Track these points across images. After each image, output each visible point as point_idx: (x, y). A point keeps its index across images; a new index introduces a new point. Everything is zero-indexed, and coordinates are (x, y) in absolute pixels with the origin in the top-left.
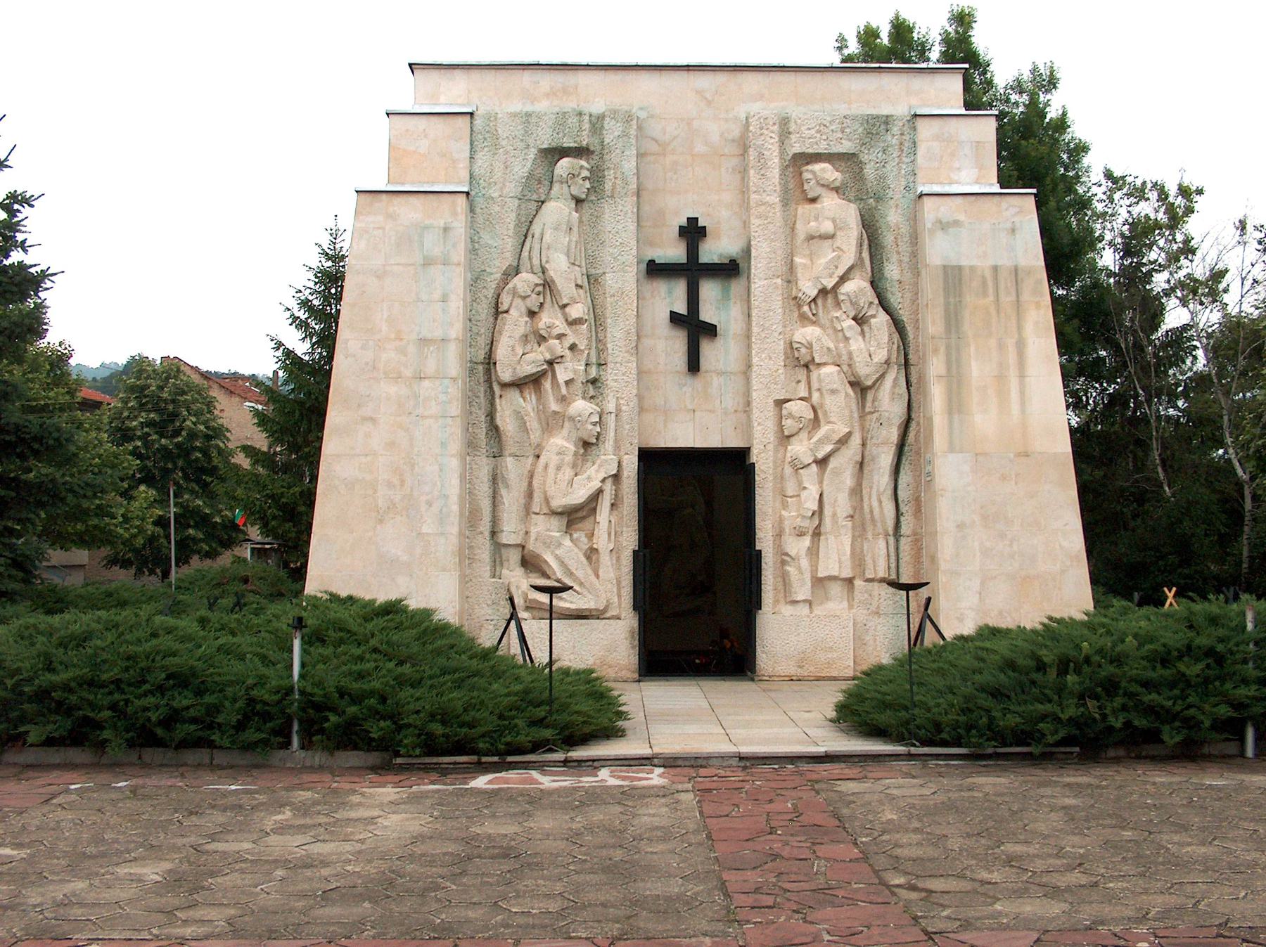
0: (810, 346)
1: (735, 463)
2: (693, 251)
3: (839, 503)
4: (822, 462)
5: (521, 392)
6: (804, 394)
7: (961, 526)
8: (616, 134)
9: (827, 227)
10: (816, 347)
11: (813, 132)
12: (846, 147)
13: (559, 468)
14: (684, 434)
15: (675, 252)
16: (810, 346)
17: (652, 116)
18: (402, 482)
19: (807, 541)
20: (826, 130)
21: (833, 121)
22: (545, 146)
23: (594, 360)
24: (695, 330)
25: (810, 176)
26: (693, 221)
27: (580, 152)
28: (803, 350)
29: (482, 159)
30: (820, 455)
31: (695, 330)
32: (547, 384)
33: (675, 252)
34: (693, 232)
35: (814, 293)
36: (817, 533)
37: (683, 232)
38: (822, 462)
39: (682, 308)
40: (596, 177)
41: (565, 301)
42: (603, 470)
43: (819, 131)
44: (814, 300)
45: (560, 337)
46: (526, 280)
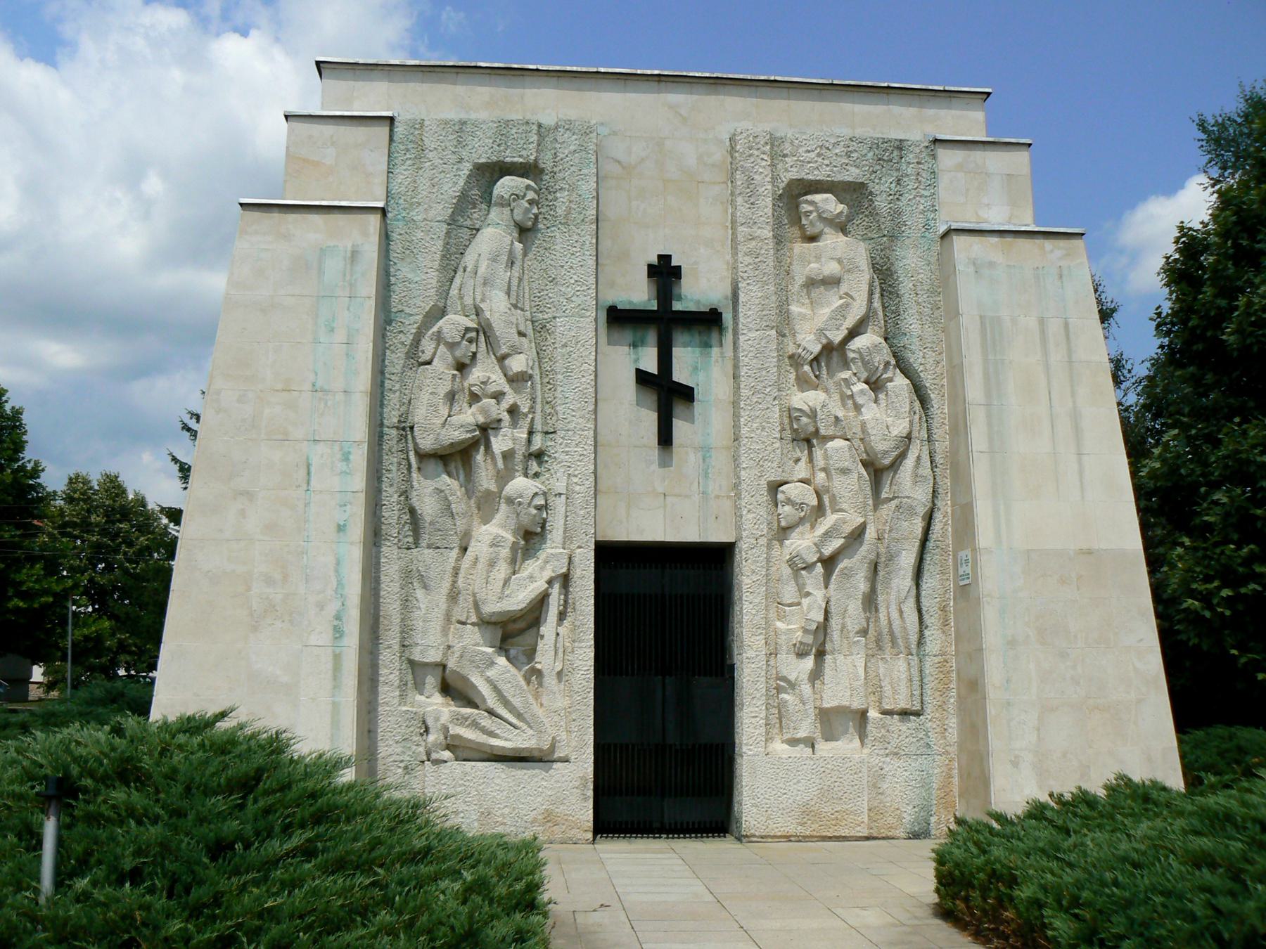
0: (813, 414)
1: (715, 560)
4: (829, 563)
5: (445, 465)
6: (803, 475)
7: (1012, 643)
8: (572, 148)
9: (832, 268)
11: (813, 155)
15: (640, 294)
16: (813, 414)
17: (615, 133)
18: (285, 578)
20: (829, 154)
21: (837, 144)
22: (482, 160)
24: (667, 395)
25: (811, 208)
26: (665, 259)
27: (528, 170)
28: (804, 420)
29: (403, 175)
30: (828, 551)
31: (667, 395)
32: (480, 457)
33: (640, 294)
34: (664, 273)
35: (816, 349)
37: (653, 271)
38: (829, 563)
39: (651, 366)
41: (504, 350)
43: (819, 155)
44: (816, 359)
45: (498, 396)
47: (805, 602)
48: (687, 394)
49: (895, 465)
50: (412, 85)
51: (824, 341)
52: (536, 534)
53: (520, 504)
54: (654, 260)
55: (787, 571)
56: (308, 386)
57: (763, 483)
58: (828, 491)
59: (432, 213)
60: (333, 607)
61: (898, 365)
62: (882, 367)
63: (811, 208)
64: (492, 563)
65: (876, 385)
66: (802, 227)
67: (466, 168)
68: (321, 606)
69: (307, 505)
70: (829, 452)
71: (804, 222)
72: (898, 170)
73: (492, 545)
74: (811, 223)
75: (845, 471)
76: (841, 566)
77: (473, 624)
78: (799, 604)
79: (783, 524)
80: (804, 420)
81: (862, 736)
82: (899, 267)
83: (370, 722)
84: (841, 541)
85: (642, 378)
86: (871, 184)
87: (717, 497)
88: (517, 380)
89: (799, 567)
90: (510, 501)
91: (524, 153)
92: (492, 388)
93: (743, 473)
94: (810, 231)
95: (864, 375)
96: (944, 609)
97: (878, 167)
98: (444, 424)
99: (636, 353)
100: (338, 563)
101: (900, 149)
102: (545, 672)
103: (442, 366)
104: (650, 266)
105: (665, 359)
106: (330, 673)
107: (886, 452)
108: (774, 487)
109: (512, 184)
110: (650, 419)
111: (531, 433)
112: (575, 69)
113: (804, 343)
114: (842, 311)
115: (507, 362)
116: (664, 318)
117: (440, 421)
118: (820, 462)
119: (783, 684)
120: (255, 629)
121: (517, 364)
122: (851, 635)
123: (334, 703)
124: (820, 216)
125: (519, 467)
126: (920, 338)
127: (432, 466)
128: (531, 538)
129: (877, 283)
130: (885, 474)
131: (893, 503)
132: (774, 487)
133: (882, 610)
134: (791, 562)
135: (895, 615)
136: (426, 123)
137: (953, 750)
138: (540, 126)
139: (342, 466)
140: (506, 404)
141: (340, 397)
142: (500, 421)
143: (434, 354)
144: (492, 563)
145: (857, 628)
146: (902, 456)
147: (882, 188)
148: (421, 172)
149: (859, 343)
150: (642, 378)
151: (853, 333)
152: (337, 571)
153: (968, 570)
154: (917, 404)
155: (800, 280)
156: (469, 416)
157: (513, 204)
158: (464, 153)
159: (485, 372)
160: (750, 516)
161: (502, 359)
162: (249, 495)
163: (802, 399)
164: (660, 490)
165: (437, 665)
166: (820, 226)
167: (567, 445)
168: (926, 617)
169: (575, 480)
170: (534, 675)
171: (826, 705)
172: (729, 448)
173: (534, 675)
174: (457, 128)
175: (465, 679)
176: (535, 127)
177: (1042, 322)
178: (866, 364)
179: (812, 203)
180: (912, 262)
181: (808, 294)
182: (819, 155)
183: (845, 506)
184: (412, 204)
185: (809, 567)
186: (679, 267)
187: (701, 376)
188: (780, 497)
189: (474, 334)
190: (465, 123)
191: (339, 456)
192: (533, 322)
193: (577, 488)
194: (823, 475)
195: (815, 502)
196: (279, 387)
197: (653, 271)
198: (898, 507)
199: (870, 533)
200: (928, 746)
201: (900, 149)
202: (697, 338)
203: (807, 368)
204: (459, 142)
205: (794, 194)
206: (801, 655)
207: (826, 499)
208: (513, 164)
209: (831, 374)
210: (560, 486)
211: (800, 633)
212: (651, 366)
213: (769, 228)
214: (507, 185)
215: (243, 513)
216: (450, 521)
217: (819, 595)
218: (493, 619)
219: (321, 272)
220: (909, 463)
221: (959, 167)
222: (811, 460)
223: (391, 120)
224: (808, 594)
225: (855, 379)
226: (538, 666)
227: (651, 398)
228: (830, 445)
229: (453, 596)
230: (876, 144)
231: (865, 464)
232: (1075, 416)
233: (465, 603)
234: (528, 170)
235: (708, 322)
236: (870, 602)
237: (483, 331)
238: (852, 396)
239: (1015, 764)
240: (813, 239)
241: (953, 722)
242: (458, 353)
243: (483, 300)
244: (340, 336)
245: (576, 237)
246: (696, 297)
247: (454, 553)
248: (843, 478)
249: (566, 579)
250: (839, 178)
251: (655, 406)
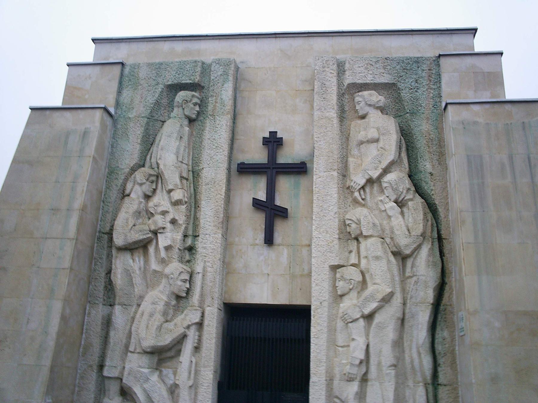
0: (358, 223)
2: (272, 156)
3: (384, 353)
4: (369, 317)
6: (353, 259)
8: (219, 73)
9: (373, 133)
11: (362, 69)
14: (260, 292)
19: (354, 387)
21: (378, 61)
22: (169, 83)
23: (190, 232)
24: (272, 213)
25: (360, 99)
26: (273, 134)
28: (354, 226)
29: (126, 94)
31: (272, 213)
32: (151, 249)
33: (257, 155)
34: (273, 142)
36: (364, 379)
37: (266, 142)
38: (369, 317)
39: (262, 196)
40: (202, 104)
41: (170, 187)
44: (363, 188)
47: (353, 344)
48: (283, 213)
51: (367, 177)
52: (183, 297)
54: (267, 135)
58: (368, 272)
62: (405, 191)
65: (400, 204)
66: (356, 111)
67: (160, 87)
72: (416, 74)
74: (362, 108)
75: (377, 258)
77: (139, 353)
78: (348, 346)
80: (354, 226)
82: (416, 131)
85: (257, 204)
86: (399, 84)
91: (192, 78)
92: (160, 209)
93: (313, 260)
94: (361, 113)
95: (394, 197)
97: (403, 74)
107: (407, 246)
111: (185, 236)
115: (172, 194)
118: (363, 253)
122: (384, 368)
125: (176, 256)
126: (431, 174)
128: (180, 299)
129: (403, 141)
130: (408, 260)
133: (407, 351)
135: (415, 355)
136: (141, 65)
138: (203, 63)
140: (169, 217)
143: (132, 189)
144: (151, 315)
145: (389, 363)
148: (136, 91)
149: (390, 177)
150: (257, 204)
151: (386, 171)
154: (430, 216)
155: (355, 143)
157: (184, 106)
158: (160, 80)
160: (317, 288)
164: (266, 272)
165: (117, 378)
166: (367, 109)
168: (439, 357)
174: (157, 67)
176: (200, 64)
178: (395, 190)
183: (377, 281)
184: (129, 109)
189: (154, 178)
190: (162, 64)
192: (193, 172)
195: (360, 278)
197: (266, 142)
203: (356, 194)
206: (350, 380)
207: (367, 276)
208: (187, 84)
211: (348, 367)
212: (262, 196)
213: (334, 111)
217: (360, 342)
218: (148, 350)
223: (122, 64)
225: (387, 200)
230: (401, 61)
231: (394, 254)
235: (300, 169)
236: (398, 344)
240: (363, 117)
243: (160, 159)
247: (135, 307)
249: (200, 325)
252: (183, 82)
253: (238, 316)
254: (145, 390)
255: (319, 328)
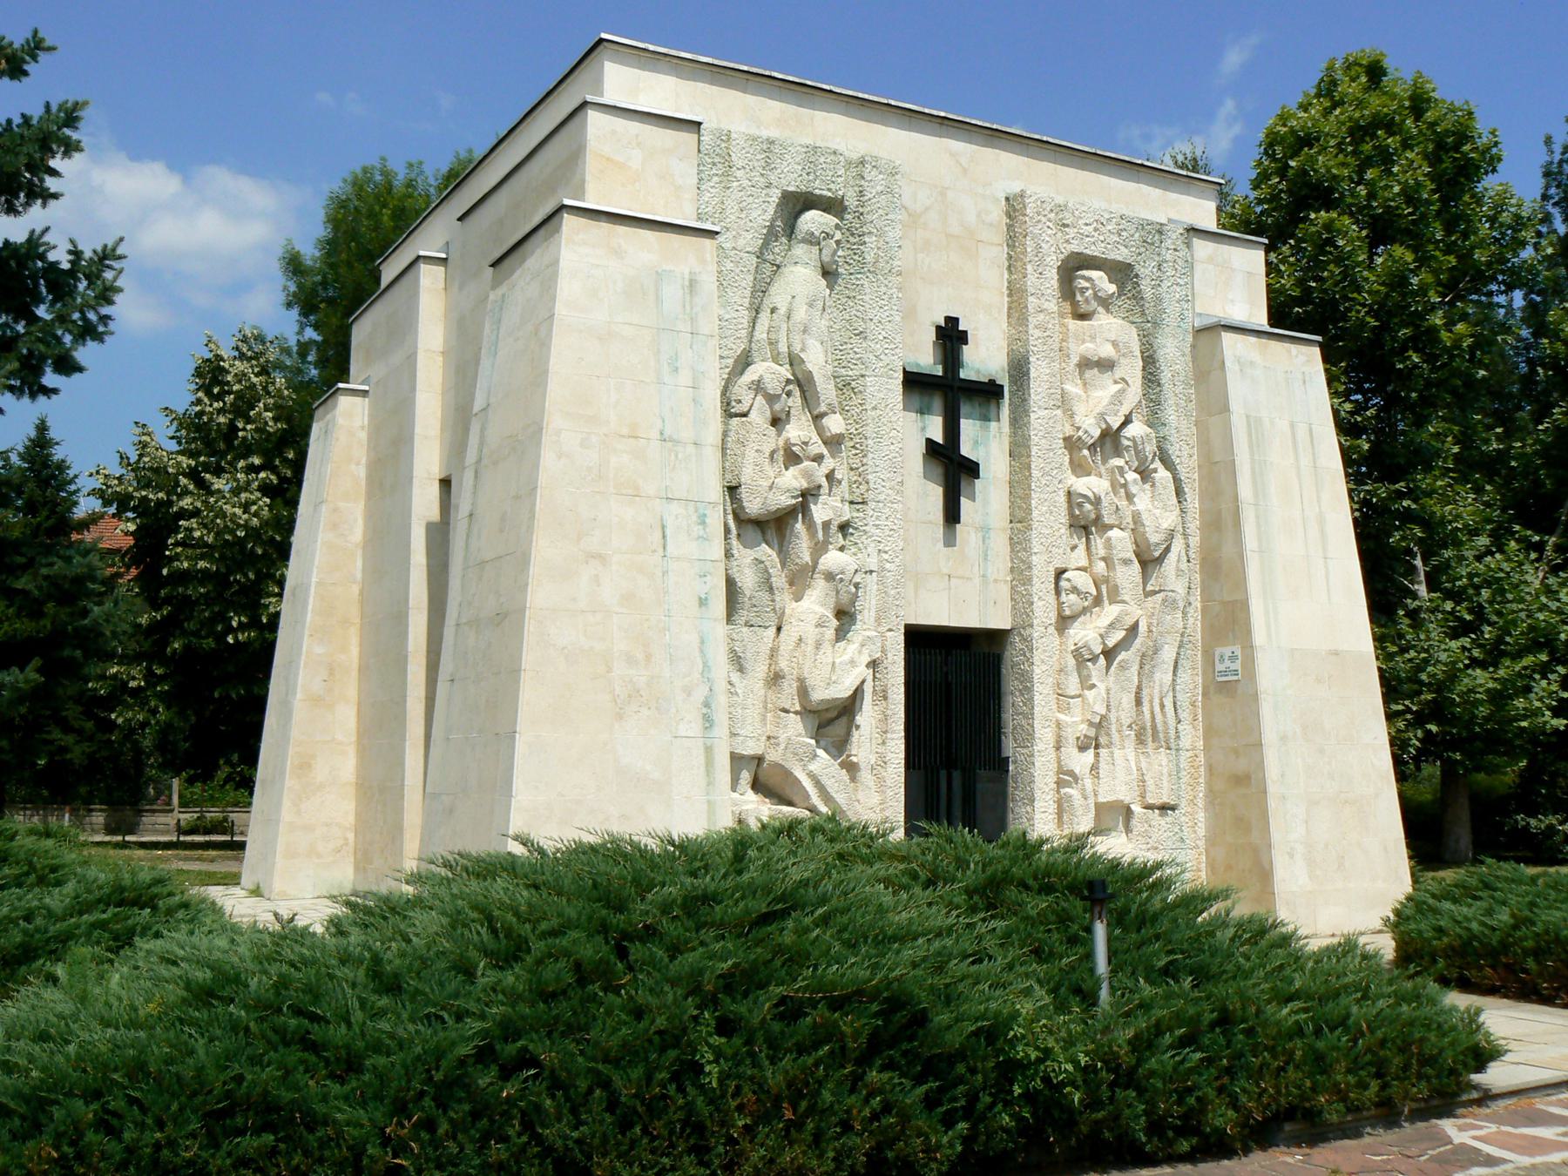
0: (1097, 501)
4: (1109, 654)
5: (763, 533)
6: (1084, 562)
7: (1284, 739)
8: (879, 188)
9: (1107, 351)
10: (1105, 503)
11: (1090, 229)
12: (1121, 254)
13: (818, 645)
16: (1097, 501)
18: (648, 657)
20: (1103, 229)
21: (1109, 220)
22: (791, 189)
24: (952, 469)
25: (1087, 285)
26: (952, 321)
27: (833, 206)
28: (1088, 506)
30: (1111, 643)
31: (952, 469)
32: (799, 526)
34: (951, 336)
35: (1097, 433)
38: (1109, 654)
41: (823, 408)
42: (865, 651)
43: (1096, 230)
45: (818, 459)
46: (769, 371)
47: (1090, 694)
48: (972, 469)
49: (1160, 560)
50: (700, 85)
53: (842, 580)
55: (1072, 662)
56: (655, 434)
57: (1052, 569)
59: (741, 242)
60: (701, 693)
61: (1161, 460)
63: (1087, 285)
64: (818, 645)
65: (1145, 474)
68: (688, 691)
69: (665, 573)
70: (1113, 542)
71: (1079, 297)
73: (819, 625)
75: (1126, 562)
76: (1119, 658)
77: (796, 713)
79: (1068, 613)
81: (1128, 830)
83: (1242, 824)
84: (1123, 633)
87: (996, 581)
88: (834, 443)
89: (1082, 658)
90: (830, 577)
91: (832, 186)
94: (1084, 308)
96: (1193, 704)
98: (771, 488)
99: (923, 421)
100: (702, 642)
101: (1160, 232)
102: (862, 766)
103: (759, 415)
104: (938, 328)
105: (952, 430)
106: (703, 769)
108: (1060, 573)
109: (822, 220)
110: (936, 493)
112: (866, 96)
113: (1084, 426)
114: (1118, 398)
116: (948, 386)
117: (766, 484)
119: (1065, 777)
120: (620, 717)
121: (835, 424)
123: (709, 802)
124: (1095, 294)
127: (752, 533)
131: (1159, 597)
132: (1060, 573)
134: (1077, 654)
135: (1157, 709)
136: (734, 136)
137: (1201, 843)
139: (697, 530)
141: (691, 449)
142: (820, 487)
145: (1129, 721)
146: (1167, 550)
147: (1146, 270)
152: (702, 651)
153: (1237, 665)
155: (1075, 360)
156: (793, 479)
159: (799, 430)
160: (1041, 603)
161: (817, 418)
162: (601, 558)
163: (1083, 485)
164: (945, 571)
165: (753, 758)
166: (1094, 304)
167: (878, 518)
169: (886, 556)
170: (851, 768)
171: (1101, 799)
172: (1004, 530)
173: (851, 768)
175: (788, 774)
177: (1292, 425)
179: (1088, 279)
180: (1174, 352)
181: (1081, 374)
182: (1096, 230)
183: (1126, 598)
185: (1094, 659)
186: (965, 332)
187: (982, 450)
188: (1063, 584)
190: (773, 142)
191: (694, 518)
193: (888, 566)
194: (1103, 564)
196: (625, 431)
198: (1164, 601)
199: (1143, 628)
200: (1182, 840)
201: (1160, 232)
202: (977, 410)
204: (768, 164)
205: (1073, 266)
206: (1082, 748)
207: (1104, 588)
209: (1104, 461)
210: (873, 563)
214: (813, 220)
215: (596, 580)
216: (766, 596)
219: (658, 300)
220: (1172, 557)
221: (1210, 260)
222: (1088, 548)
224: (1093, 686)
226: (854, 759)
227: (938, 471)
228: (1110, 533)
229: (775, 679)
230: (1142, 225)
232: (1321, 521)
233: (789, 688)
234: (833, 206)
235: (988, 392)
237: (803, 383)
238: (1125, 486)
239: (1291, 856)
241: (1201, 816)
242: (777, 407)
243: (803, 350)
244: (685, 378)
245: (883, 289)
246: (977, 366)
248: (1124, 569)
250: (1112, 256)
251: (941, 479)
252: (817, 192)
253: (923, 643)
254: (812, 776)
255: (1044, 668)
